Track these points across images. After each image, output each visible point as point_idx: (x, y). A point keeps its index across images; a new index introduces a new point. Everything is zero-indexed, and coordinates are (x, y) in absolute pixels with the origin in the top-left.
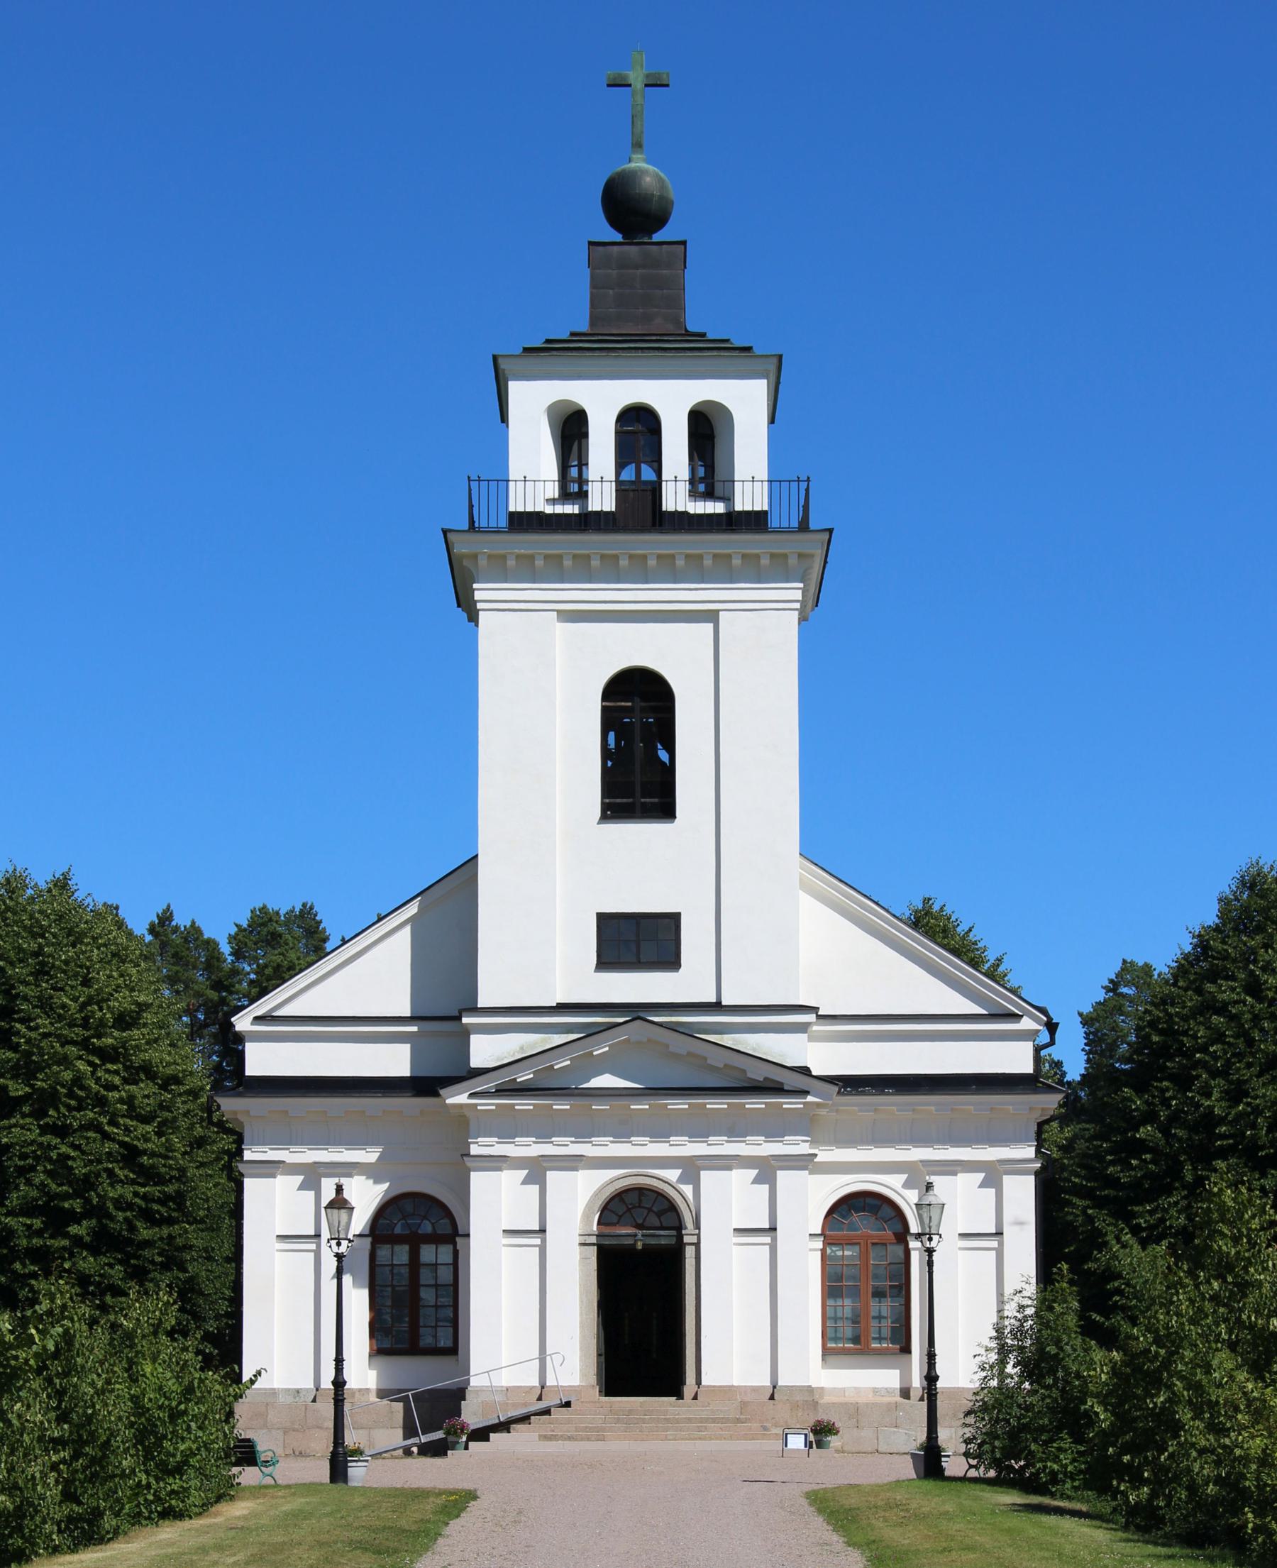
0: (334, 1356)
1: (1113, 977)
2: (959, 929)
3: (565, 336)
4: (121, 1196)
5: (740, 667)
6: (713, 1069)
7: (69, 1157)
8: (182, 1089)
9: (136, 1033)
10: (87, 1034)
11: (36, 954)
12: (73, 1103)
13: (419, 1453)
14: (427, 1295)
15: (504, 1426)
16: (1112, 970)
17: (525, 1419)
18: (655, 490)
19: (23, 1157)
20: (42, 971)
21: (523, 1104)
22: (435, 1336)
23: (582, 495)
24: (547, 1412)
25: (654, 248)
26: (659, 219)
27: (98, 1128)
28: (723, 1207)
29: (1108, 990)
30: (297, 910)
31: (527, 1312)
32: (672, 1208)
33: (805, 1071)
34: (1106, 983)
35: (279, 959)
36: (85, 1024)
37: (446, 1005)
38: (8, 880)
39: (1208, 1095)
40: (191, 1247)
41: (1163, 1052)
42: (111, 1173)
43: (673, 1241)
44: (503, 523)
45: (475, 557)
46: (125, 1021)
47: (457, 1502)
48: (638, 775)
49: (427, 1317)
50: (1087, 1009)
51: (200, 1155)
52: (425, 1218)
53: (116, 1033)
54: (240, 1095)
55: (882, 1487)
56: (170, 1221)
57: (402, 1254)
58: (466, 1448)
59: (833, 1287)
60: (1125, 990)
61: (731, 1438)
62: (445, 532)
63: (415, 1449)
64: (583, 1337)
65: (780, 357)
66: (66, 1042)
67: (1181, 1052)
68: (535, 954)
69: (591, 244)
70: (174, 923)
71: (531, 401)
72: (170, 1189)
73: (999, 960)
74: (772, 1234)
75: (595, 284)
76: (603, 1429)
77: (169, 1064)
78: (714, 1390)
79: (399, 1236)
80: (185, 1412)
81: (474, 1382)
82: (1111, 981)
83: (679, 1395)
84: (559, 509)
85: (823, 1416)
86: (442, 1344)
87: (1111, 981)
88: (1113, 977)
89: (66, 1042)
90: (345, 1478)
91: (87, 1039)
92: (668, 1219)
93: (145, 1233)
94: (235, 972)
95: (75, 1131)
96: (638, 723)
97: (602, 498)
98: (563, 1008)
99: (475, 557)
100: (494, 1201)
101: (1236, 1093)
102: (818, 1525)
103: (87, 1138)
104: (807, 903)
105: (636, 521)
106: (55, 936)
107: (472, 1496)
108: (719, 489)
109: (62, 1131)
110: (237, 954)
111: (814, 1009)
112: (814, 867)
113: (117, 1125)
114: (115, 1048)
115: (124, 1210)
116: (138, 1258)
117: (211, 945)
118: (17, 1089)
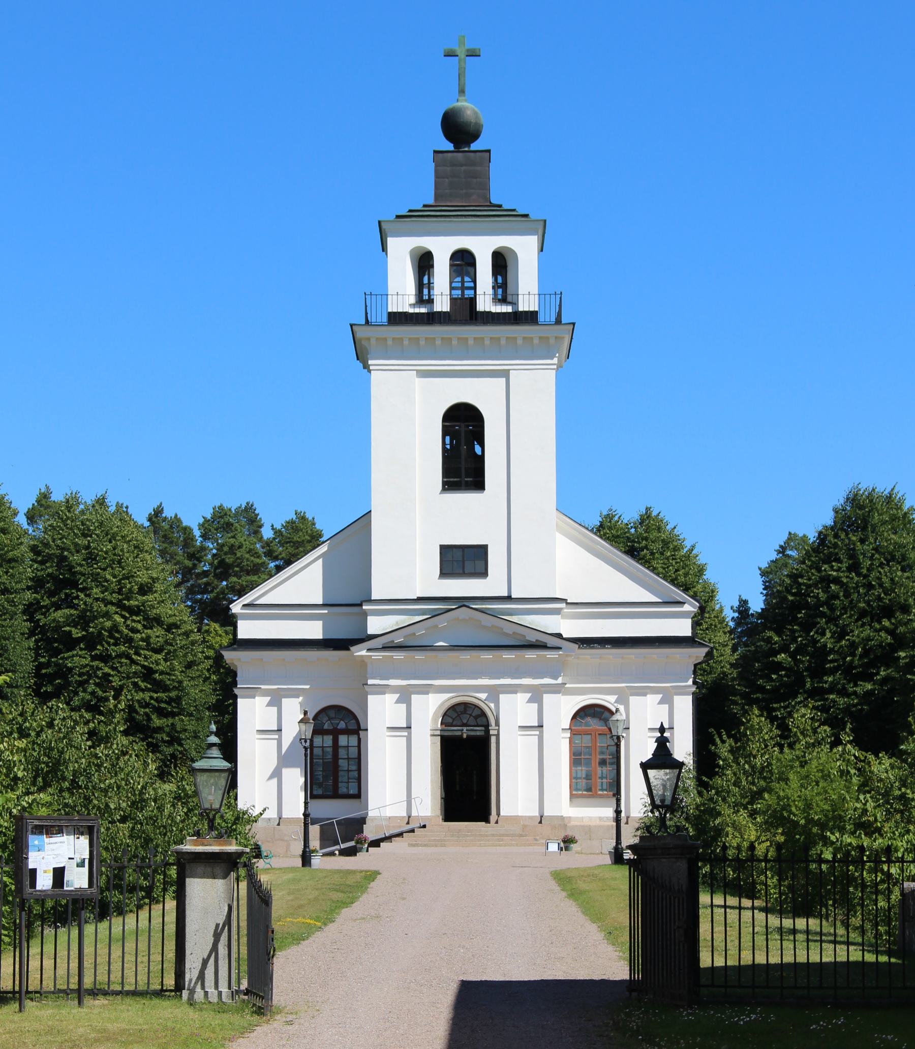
0: (303, 800)
1: (783, 544)
2: (668, 527)
3: (420, 207)
4: (143, 699)
5: (522, 403)
6: (507, 635)
7: (109, 675)
8: (180, 631)
9: (150, 597)
10: (120, 597)
11: (87, 547)
12: (112, 641)
13: (340, 854)
14: (343, 763)
15: (388, 839)
16: (782, 539)
17: (400, 835)
18: (473, 301)
19: (80, 675)
20: (91, 558)
21: (398, 655)
22: (348, 788)
23: (430, 301)
24: (412, 831)
25: (472, 154)
26: (475, 136)
27: (128, 657)
28: (512, 714)
29: (779, 552)
30: (243, 507)
31: (400, 774)
32: (483, 714)
33: (559, 636)
34: (778, 548)
35: (232, 541)
36: (120, 592)
37: (350, 598)
38: (68, 501)
39: (823, 634)
40: (185, 730)
41: (795, 607)
42: (135, 685)
43: (482, 733)
44: (385, 319)
45: (369, 339)
46: (145, 590)
47: (372, 875)
48: (463, 467)
49: (342, 776)
50: (764, 565)
51: (193, 673)
52: (342, 720)
53: (139, 597)
54: (235, 650)
55: (590, 868)
56: (173, 715)
57: (328, 740)
58: (367, 851)
59: (576, 758)
60: (789, 552)
61: (517, 845)
62: (351, 326)
63: (337, 852)
64: (433, 789)
65: (545, 221)
66: (107, 603)
67: (807, 606)
68: (403, 568)
69: (435, 152)
70: (164, 515)
71: (401, 249)
72: (173, 694)
73: (693, 547)
74: (540, 729)
75: (438, 175)
76: (444, 841)
77: (170, 616)
78: (507, 818)
79: (327, 730)
80: (235, 830)
81: (371, 814)
82: (781, 547)
83: (487, 821)
84: (417, 310)
85: (570, 833)
86: (351, 792)
87: (781, 547)
88: (783, 544)
89: (107, 603)
90: (310, 865)
91: (120, 601)
92: (481, 721)
93: (157, 722)
94: (203, 549)
95: (113, 659)
96: (463, 432)
97: (442, 304)
98: (420, 600)
99: (369, 339)
100: (381, 712)
101: (841, 634)
102: (553, 884)
103: (121, 663)
104: (561, 539)
105: (461, 319)
106: (97, 535)
107: (377, 873)
108: (509, 299)
109: (105, 658)
110: (205, 536)
111: (564, 600)
112: (564, 517)
113: (139, 655)
114: (138, 607)
115: (145, 707)
116: (153, 738)
117: (187, 530)
118: (77, 633)
